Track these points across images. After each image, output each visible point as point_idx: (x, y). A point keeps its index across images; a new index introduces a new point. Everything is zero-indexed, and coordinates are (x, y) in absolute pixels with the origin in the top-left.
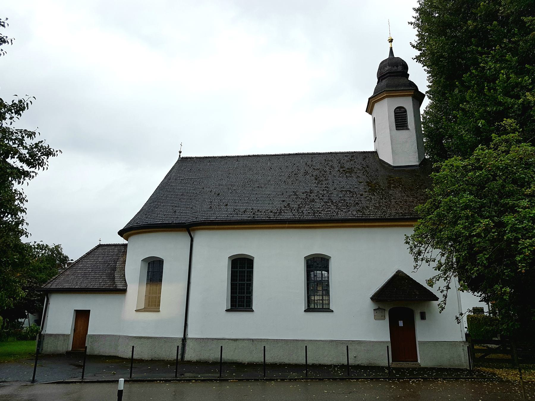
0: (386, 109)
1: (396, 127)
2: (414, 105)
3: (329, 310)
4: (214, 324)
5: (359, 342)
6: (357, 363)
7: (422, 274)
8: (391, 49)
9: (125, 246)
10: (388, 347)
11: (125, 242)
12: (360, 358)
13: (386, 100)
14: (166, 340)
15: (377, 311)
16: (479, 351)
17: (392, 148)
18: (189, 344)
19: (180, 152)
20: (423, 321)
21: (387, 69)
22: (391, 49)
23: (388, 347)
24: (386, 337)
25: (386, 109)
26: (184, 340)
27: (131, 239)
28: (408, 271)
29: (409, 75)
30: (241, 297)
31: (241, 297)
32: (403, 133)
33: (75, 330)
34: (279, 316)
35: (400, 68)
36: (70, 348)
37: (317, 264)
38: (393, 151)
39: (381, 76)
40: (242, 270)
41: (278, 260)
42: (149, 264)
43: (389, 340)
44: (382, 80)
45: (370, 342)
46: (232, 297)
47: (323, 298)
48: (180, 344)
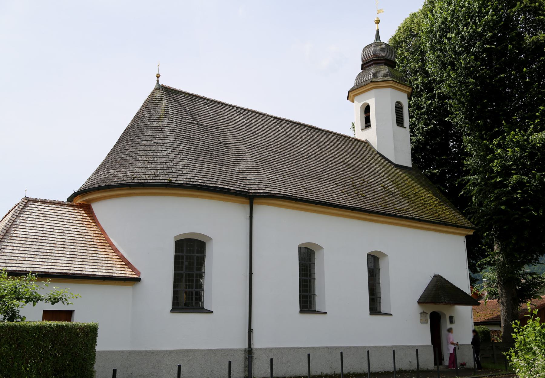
4: (282, 328)
8: (378, 31)
18: (255, 355)
19: (158, 76)
21: (383, 54)
22: (378, 31)
39: (365, 65)
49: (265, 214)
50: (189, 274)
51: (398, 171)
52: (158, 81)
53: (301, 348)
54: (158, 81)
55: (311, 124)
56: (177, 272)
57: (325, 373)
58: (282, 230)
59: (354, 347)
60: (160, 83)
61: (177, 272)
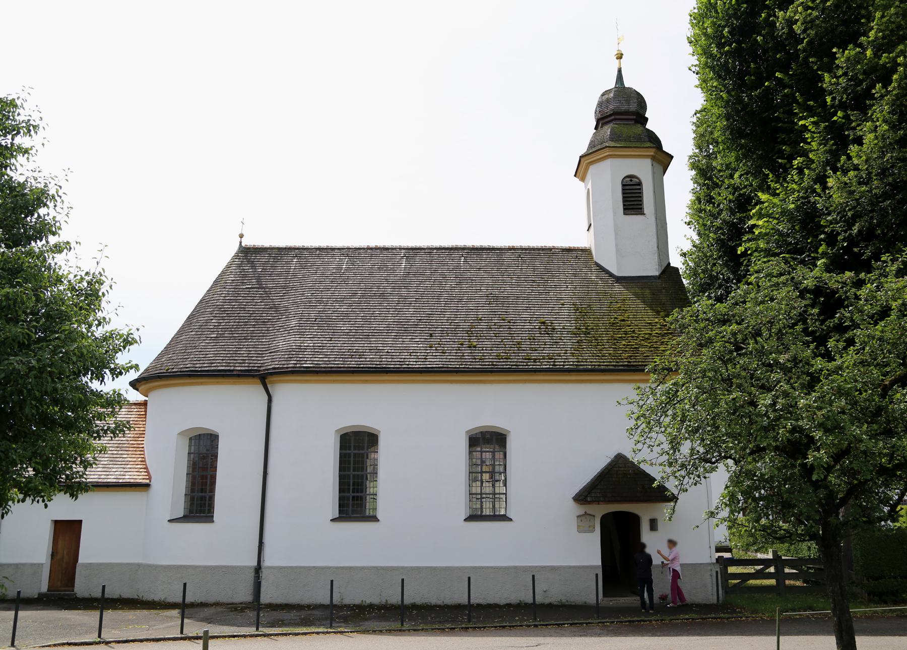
0: (611, 172)
1: (624, 209)
2: (654, 173)
3: (505, 518)
4: (309, 540)
5: (553, 569)
6: (547, 601)
7: (652, 460)
8: (620, 71)
9: (145, 404)
10: (597, 575)
11: (145, 398)
12: (551, 592)
13: (609, 162)
14: (227, 570)
15: (583, 518)
16: (735, 576)
17: (617, 245)
18: (264, 574)
19: (241, 236)
20: (654, 533)
21: (611, 107)
22: (620, 71)
23: (597, 575)
24: (594, 557)
25: (611, 172)
26: (258, 569)
27: (151, 395)
28: (629, 455)
29: (647, 119)
30: (354, 497)
31: (354, 497)
32: (634, 220)
33: (53, 555)
34: (422, 525)
35: (633, 107)
36: (44, 588)
37: (488, 443)
38: (618, 251)
39: (601, 121)
40: (357, 453)
41: (422, 432)
42: (191, 439)
43: (599, 562)
44: (603, 125)
45: (570, 567)
46: (341, 499)
47: (494, 457)
48: (251, 575)
49: (290, 396)
50: (358, 475)
51: (618, 288)
52: (241, 243)
53: (329, 568)
54: (241, 243)
55: (470, 243)
56: (343, 473)
57: (368, 602)
58: (314, 416)
59: (427, 568)
60: (243, 245)
61: (343, 473)
